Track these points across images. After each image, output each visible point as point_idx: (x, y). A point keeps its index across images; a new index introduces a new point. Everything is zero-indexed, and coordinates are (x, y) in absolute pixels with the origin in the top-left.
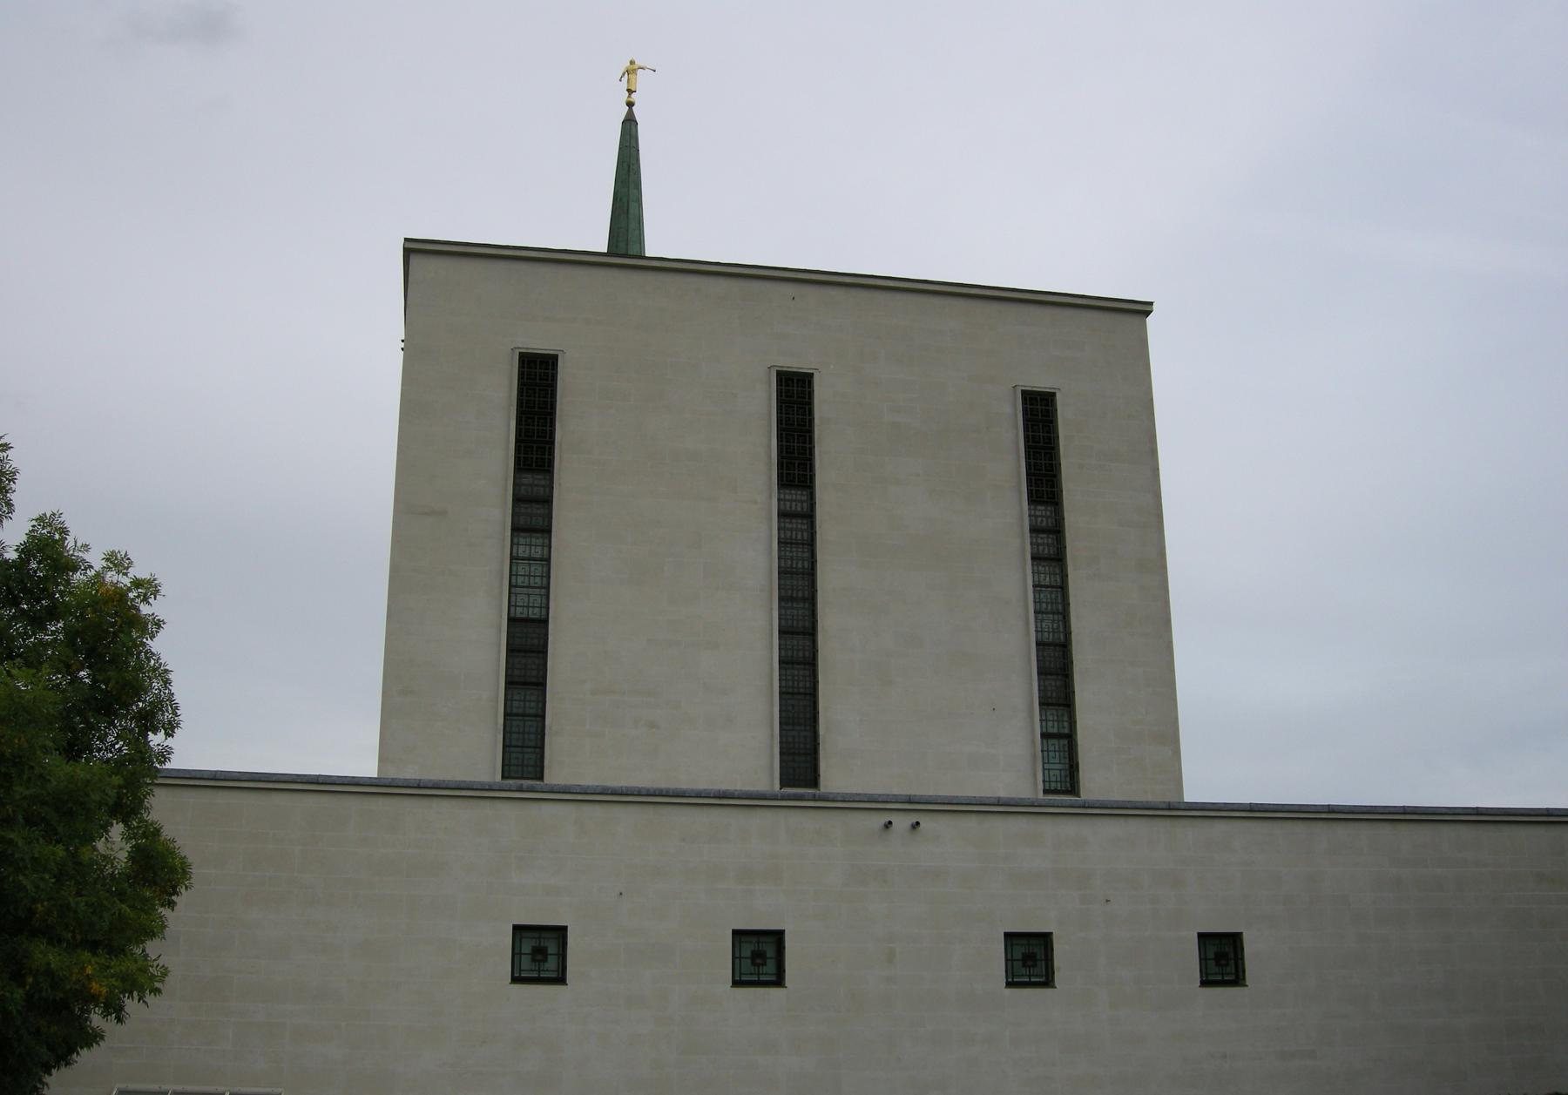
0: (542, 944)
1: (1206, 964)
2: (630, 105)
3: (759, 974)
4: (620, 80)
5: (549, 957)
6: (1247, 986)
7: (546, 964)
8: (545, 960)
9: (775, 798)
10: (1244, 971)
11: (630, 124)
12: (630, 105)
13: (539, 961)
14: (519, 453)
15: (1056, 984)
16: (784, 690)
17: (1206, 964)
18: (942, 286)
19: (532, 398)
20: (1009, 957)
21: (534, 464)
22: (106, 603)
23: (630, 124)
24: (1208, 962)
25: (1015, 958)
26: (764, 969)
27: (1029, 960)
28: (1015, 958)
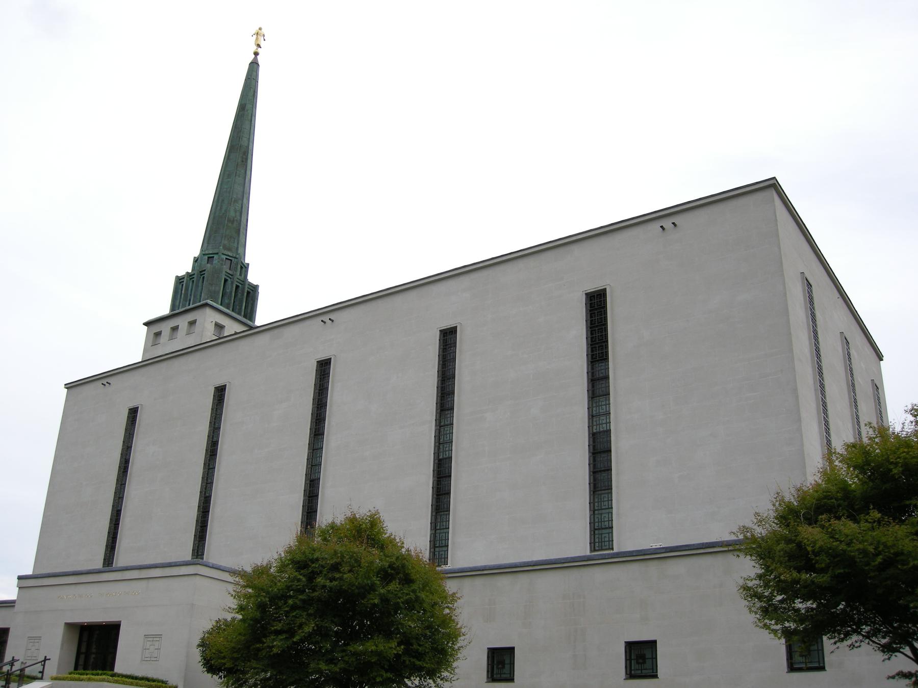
0: (642, 652)
1: (511, 661)
2: (256, 54)
3: (501, 674)
4: (264, 40)
5: (647, 660)
6: (826, 670)
7: (645, 665)
8: (644, 662)
9: (589, 558)
10: (626, 667)
11: (254, 67)
12: (256, 54)
13: (641, 663)
14: (605, 334)
15: (826, 669)
16: (610, 491)
17: (511, 661)
18: (583, 234)
19: (598, 300)
20: (654, 660)
21: (597, 340)
22: (898, 449)
23: (254, 67)
24: (651, 657)
25: (651, 660)
26: (505, 671)
27: (641, 659)
28: (651, 660)
